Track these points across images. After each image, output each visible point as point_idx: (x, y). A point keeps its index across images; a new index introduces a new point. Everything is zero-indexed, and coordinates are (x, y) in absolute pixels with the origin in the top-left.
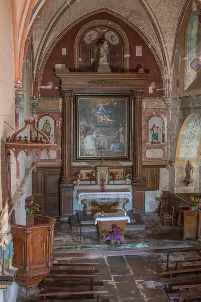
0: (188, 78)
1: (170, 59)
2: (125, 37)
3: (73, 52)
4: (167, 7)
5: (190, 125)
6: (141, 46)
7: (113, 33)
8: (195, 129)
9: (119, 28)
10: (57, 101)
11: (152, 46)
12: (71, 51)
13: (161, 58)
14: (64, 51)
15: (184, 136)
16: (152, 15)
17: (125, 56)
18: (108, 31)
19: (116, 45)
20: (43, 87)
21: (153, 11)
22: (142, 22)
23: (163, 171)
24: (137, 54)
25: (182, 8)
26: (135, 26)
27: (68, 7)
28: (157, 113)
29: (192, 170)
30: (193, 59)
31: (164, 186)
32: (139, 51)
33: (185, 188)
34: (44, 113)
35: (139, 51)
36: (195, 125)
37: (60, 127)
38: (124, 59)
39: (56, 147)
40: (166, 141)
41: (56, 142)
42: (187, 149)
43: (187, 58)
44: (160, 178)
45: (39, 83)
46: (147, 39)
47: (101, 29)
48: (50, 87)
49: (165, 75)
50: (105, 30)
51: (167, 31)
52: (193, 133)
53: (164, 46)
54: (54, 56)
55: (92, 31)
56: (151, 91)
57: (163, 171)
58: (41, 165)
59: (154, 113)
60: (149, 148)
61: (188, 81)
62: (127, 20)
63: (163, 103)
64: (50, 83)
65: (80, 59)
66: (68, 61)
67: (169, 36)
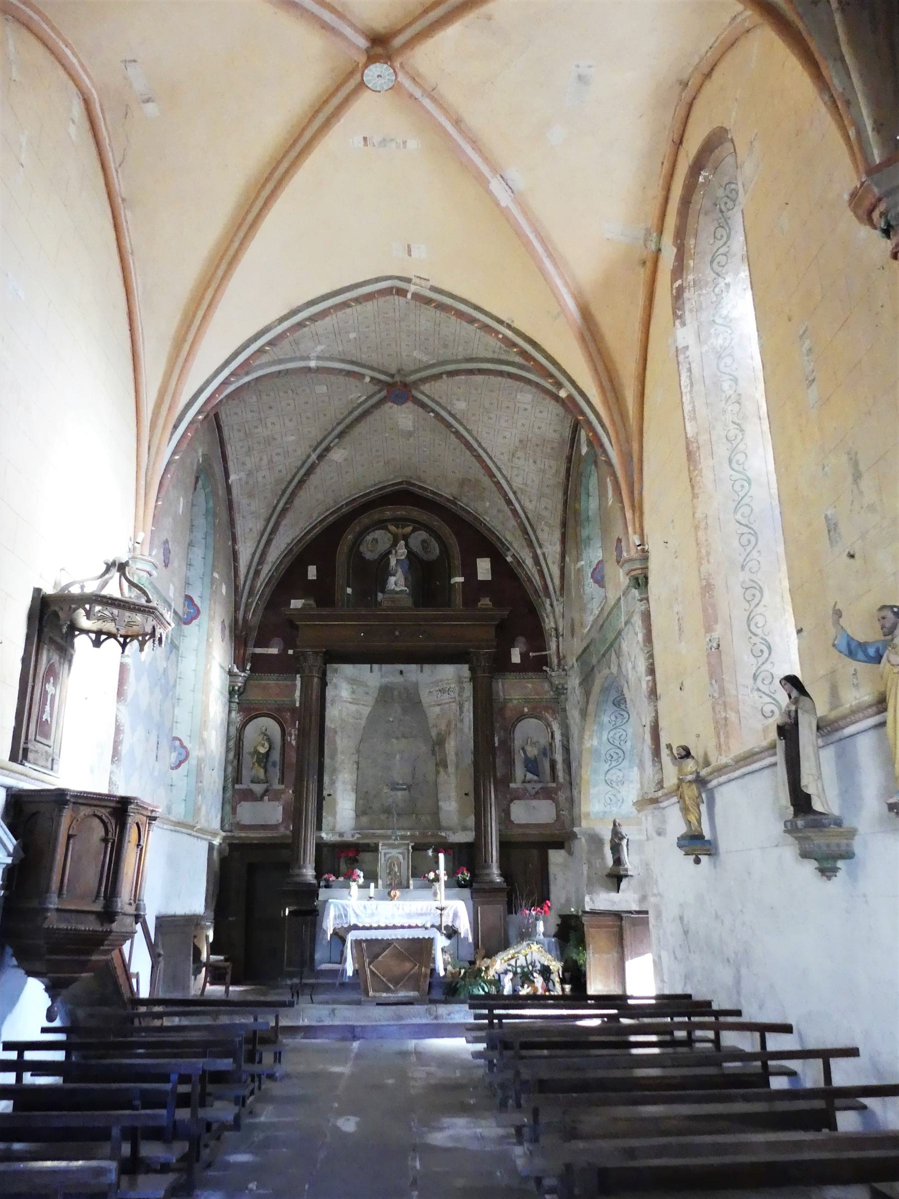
0: (589, 606)
1: (557, 581)
2: (453, 542)
4: (531, 461)
5: (605, 719)
6: (488, 559)
7: (423, 535)
8: (619, 732)
9: (436, 522)
10: (289, 683)
11: (513, 556)
13: (537, 578)
14: (312, 572)
15: (595, 752)
16: (503, 481)
17: (453, 581)
18: (413, 531)
20: (259, 651)
21: (505, 472)
22: (488, 504)
23: (556, 857)
25: (564, 457)
27: (313, 467)
28: (533, 709)
29: (624, 842)
30: (596, 562)
31: (563, 901)
32: (484, 568)
33: (613, 895)
34: (257, 710)
35: (484, 568)
36: (619, 720)
37: (294, 743)
39: (282, 792)
40: (561, 780)
41: (282, 781)
42: (609, 788)
43: (582, 563)
44: (551, 877)
45: (251, 642)
46: (502, 543)
47: (397, 527)
48: (274, 651)
49: (547, 620)
50: (410, 529)
51: (540, 518)
52: (617, 743)
53: (539, 551)
54: (288, 579)
56: (516, 658)
57: (556, 857)
58: (240, 838)
59: (526, 710)
60: (519, 799)
61: (588, 613)
62: (456, 504)
63: (546, 686)
64: (276, 640)
66: (322, 594)
67: (546, 529)
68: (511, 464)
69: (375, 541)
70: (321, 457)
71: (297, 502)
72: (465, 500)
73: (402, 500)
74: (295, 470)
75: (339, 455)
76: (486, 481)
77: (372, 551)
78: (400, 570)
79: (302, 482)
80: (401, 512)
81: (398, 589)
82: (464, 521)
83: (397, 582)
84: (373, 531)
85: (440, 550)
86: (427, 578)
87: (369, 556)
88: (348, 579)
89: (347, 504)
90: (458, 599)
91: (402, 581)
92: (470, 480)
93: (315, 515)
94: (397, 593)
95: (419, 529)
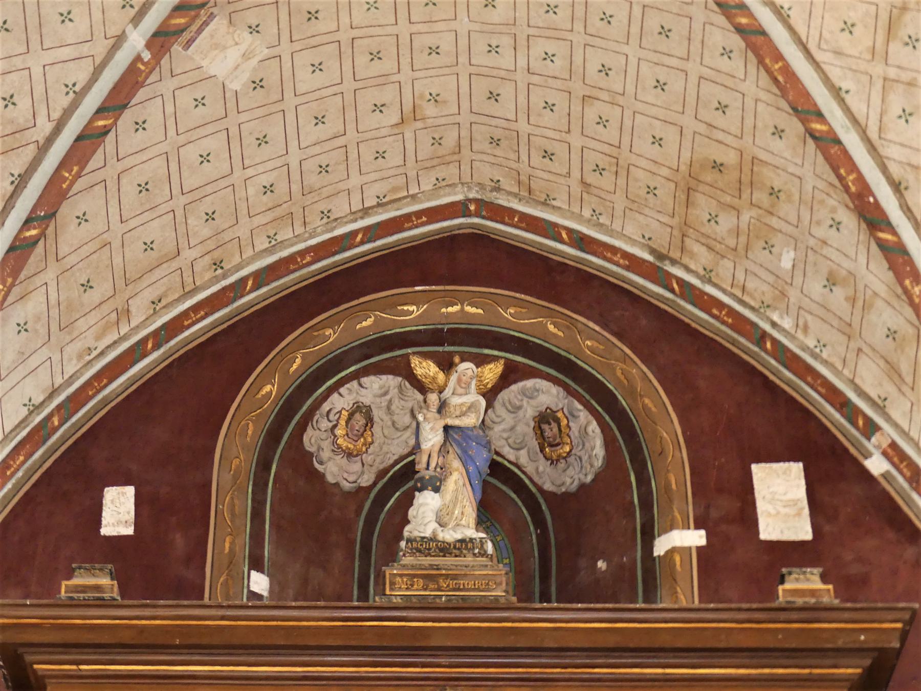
3: (197, 515)
6: (796, 469)
7: (545, 393)
11: (894, 453)
12: (175, 510)
14: (118, 510)
17: (661, 546)
19: (582, 486)
22: (786, 262)
24: (771, 528)
26: (741, 324)
32: (781, 499)
35: (781, 499)
38: (651, 575)
55: (374, 383)
62: (665, 280)
65: (259, 583)
68: (878, 69)
69: (363, 411)
70: (162, 40)
71: (70, 233)
72: (701, 257)
73: (470, 268)
74: (62, 101)
75: (233, 55)
76: (789, 158)
77: (349, 455)
78: (456, 464)
79: (89, 140)
80: (464, 308)
81: (449, 536)
82: (694, 334)
83: (444, 513)
84: (356, 376)
85: (609, 442)
86: (558, 536)
87: (337, 471)
88: (257, 538)
89: (261, 277)
90: (687, 592)
91: (468, 511)
92: (718, 167)
93: (139, 309)
94: (445, 549)
95: (533, 373)
